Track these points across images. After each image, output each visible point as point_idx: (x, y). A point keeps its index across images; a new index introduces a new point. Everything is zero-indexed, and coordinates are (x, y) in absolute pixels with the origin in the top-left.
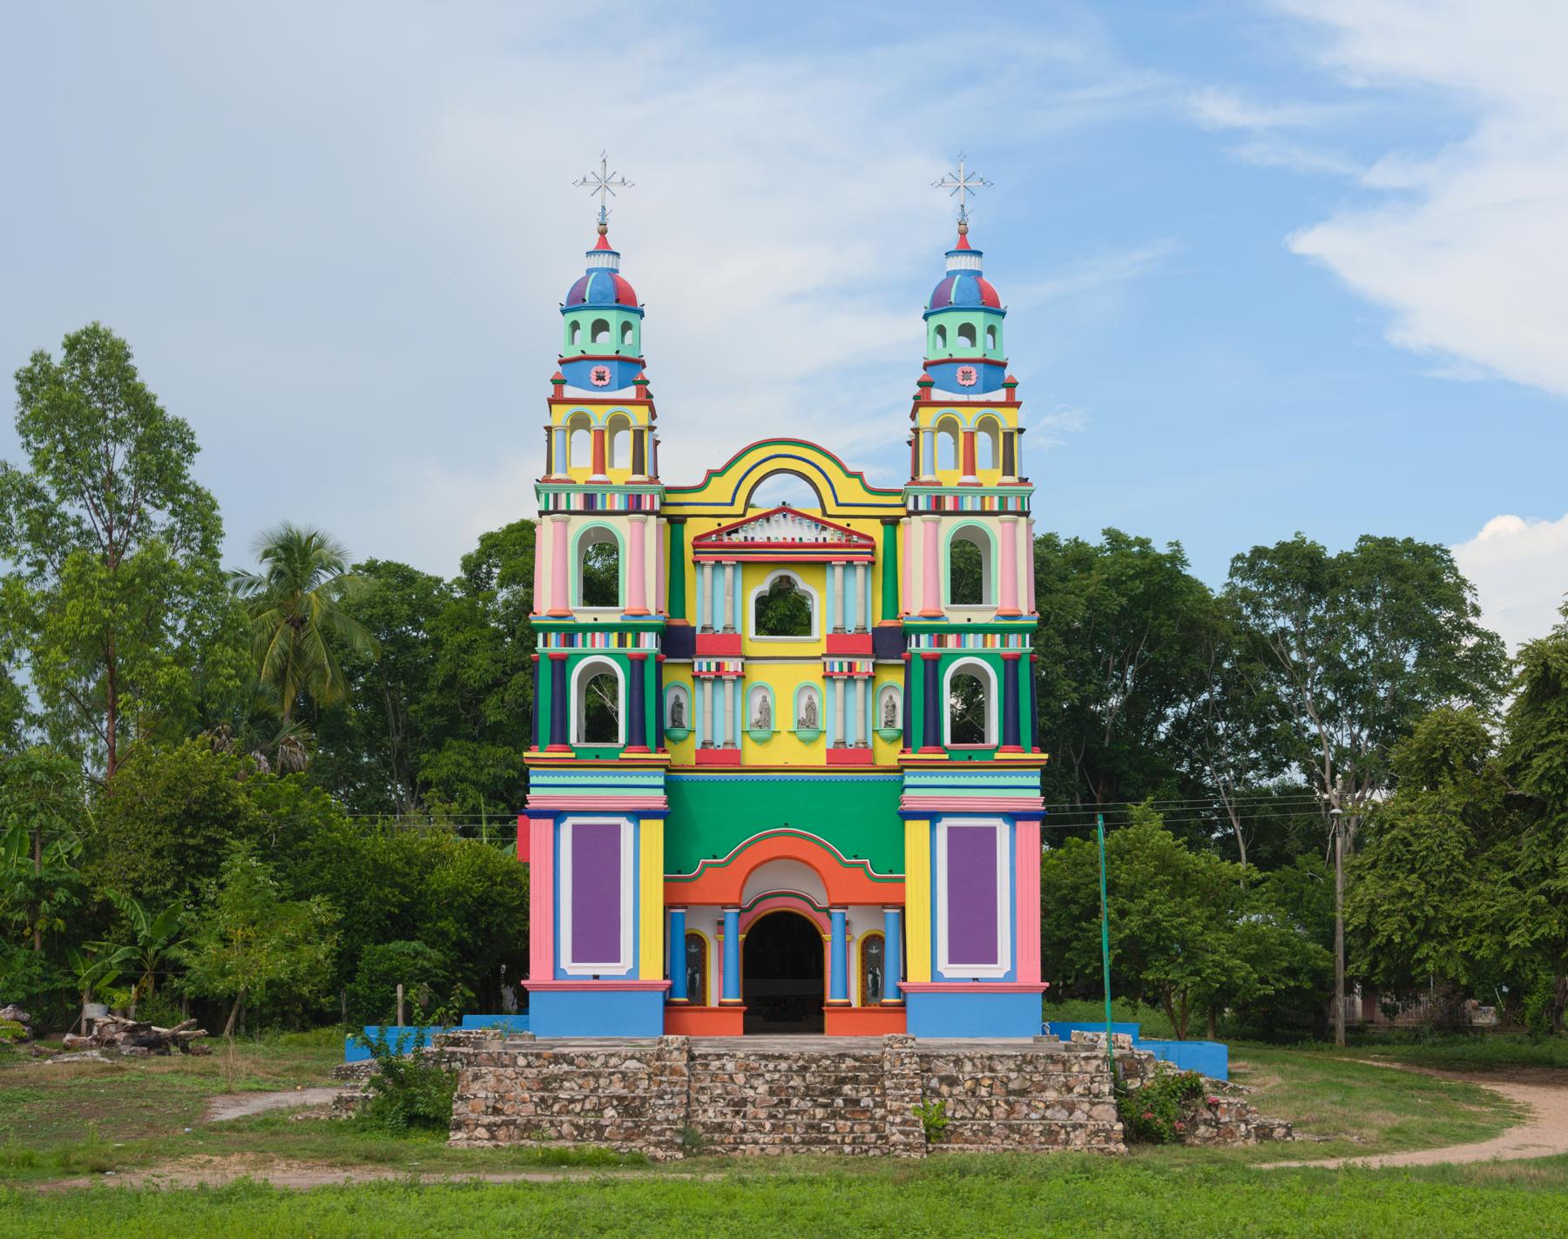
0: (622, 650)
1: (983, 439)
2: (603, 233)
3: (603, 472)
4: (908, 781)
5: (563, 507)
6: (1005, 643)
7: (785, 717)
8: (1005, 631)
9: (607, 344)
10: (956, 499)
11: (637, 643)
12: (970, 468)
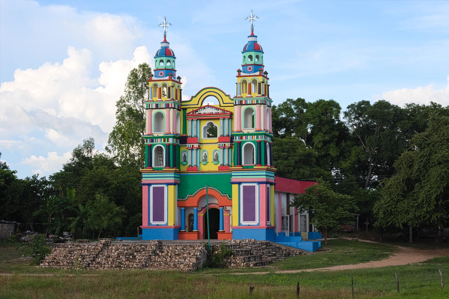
0: (165, 143)
1: (253, 85)
2: (165, 37)
3: (161, 98)
4: (233, 174)
5: (151, 107)
6: (257, 138)
7: (210, 158)
8: (257, 135)
9: (255, 60)
10: (245, 101)
11: (168, 141)
12: (250, 93)
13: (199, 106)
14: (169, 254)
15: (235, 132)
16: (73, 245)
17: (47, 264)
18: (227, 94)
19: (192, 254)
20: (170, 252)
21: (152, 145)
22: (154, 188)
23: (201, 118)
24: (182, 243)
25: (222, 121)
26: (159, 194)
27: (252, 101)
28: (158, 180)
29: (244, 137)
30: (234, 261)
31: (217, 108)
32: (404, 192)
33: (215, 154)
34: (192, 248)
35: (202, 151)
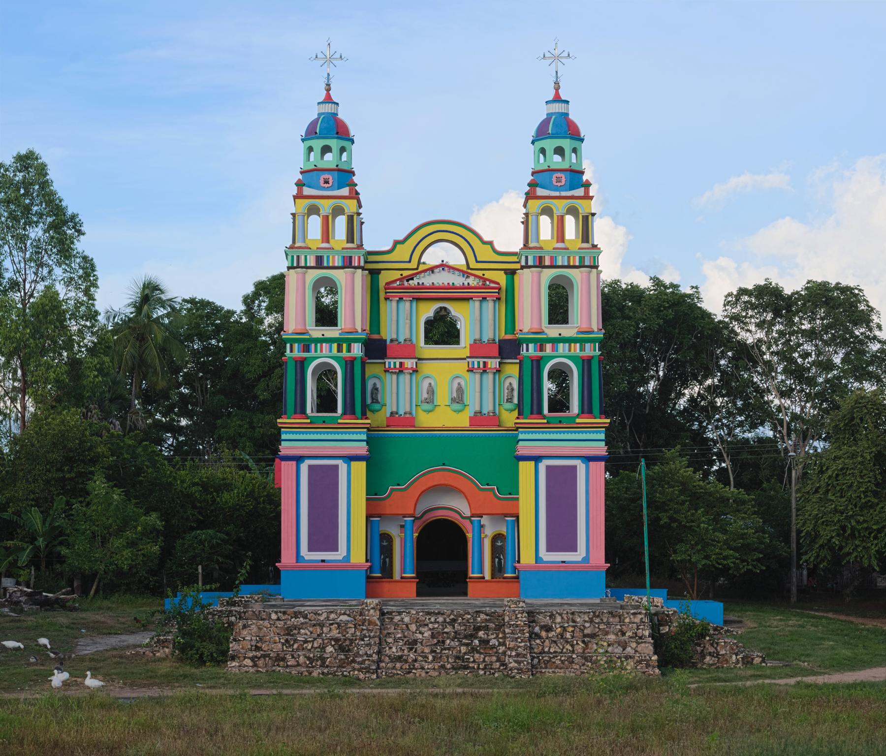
0: (340, 354)
2: (328, 90)
4: (521, 436)
5: (302, 264)
6: (582, 349)
7: (443, 396)
8: (582, 342)
10: (552, 258)
11: (349, 351)
13: (413, 264)
14: (568, 635)
15: (525, 334)
16: (284, 613)
17: (248, 662)
18: (486, 239)
19: (629, 634)
20: (571, 629)
21: (305, 359)
22: (310, 467)
23: (420, 296)
24: (426, 604)
25: (477, 304)
26: (324, 483)
27: (569, 257)
28: (325, 448)
29: (548, 347)
30: (712, 650)
31: (466, 274)
32: (877, 485)
33: (455, 386)
34: (617, 619)
35: (420, 376)
